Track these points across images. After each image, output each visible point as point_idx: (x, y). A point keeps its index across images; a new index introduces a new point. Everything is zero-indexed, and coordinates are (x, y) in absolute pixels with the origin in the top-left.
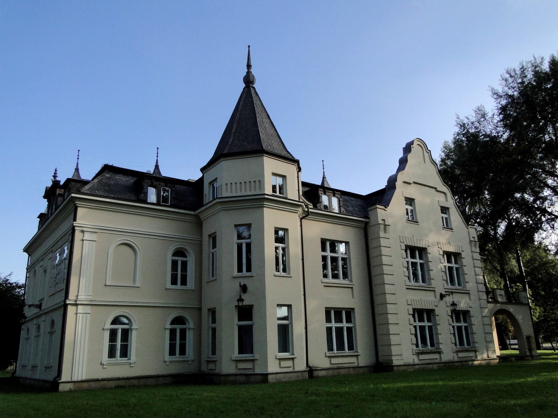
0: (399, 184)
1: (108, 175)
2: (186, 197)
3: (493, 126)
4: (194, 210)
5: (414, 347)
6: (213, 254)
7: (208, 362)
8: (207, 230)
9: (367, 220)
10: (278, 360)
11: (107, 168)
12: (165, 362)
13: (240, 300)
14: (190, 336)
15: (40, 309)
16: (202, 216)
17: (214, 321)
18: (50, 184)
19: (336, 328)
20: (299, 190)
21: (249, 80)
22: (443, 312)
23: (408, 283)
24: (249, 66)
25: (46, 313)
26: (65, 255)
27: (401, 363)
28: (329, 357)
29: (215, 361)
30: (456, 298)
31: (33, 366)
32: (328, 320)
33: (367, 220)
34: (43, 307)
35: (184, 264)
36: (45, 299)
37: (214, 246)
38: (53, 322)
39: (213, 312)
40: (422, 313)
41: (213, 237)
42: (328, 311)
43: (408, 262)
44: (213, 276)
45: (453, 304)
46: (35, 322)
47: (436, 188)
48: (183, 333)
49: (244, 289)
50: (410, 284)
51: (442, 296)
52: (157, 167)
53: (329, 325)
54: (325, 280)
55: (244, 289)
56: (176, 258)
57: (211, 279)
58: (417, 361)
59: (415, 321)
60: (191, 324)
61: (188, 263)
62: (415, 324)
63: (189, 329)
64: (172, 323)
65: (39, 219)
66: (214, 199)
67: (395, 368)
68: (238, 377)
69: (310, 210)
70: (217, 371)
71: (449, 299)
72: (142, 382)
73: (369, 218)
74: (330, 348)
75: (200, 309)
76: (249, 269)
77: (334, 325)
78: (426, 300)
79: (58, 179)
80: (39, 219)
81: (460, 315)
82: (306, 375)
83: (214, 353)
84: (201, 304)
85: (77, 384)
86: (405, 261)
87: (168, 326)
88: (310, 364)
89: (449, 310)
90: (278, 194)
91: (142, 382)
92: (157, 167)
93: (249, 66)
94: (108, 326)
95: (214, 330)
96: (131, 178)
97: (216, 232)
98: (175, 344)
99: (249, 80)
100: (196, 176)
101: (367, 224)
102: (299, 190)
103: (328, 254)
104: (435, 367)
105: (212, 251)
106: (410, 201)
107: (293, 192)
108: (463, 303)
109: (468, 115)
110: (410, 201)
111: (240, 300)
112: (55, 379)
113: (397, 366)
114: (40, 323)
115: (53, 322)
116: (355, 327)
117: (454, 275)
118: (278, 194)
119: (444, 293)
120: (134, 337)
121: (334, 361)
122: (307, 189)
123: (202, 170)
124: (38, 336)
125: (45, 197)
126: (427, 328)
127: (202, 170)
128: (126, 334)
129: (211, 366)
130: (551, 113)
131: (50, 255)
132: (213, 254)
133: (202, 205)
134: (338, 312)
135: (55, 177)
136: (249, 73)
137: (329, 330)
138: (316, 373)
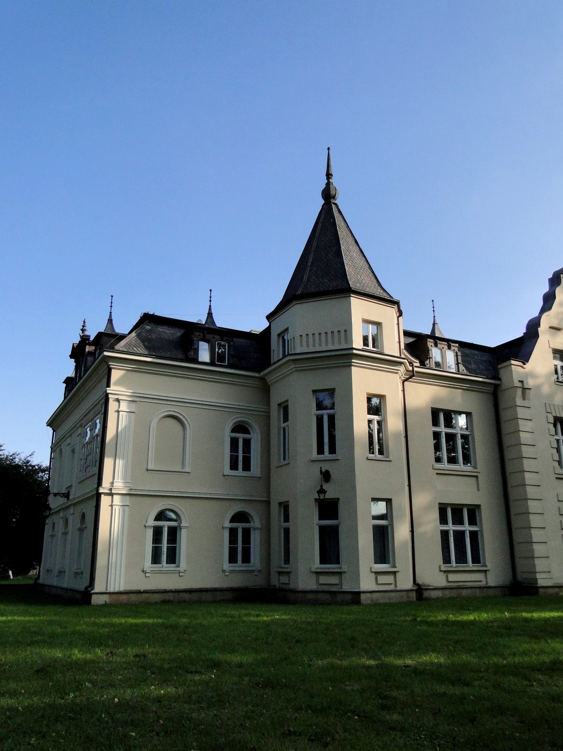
1: (148, 327)
4: (259, 371)
6: (284, 429)
7: (280, 573)
8: (276, 398)
9: (497, 382)
10: (374, 574)
13: (322, 491)
14: (256, 538)
15: (68, 499)
18: (77, 340)
20: (399, 342)
21: (328, 195)
24: (329, 175)
25: (74, 505)
28: (445, 572)
29: (288, 573)
33: (497, 382)
34: (71, 497)
35: (247, 443)
37: (286, 419)
39: (285, 507)
41: (285, 408)
44: (284, 459)
48: (247, 533)
52: (210, 315)
53: (445, 528)
54: (438, 466)
55: (326, 476)
57: (285, 462)
60: (256, 523)
61: (252, 441)
63: (254, 529)
64: (232, 521)
65: (73, 360)
66: (284, 356)
70: (292, 586)
73: (500, 379)
74: (447, 559)
75: (268, 503)
76: (332, 450)
77: (451, 527)
79: (87, 333)
82: (413, 595)
85: (114, 596)
86: (553, 440)
87: (227, 524)
88: (419, 581)
90: (371, 347)
92: (210, 315)
93: (329, 175)
95: (287, 531)
97: (287, 401)
98: (236, 548)
99: (328, 195)
100: (258, 325)
101: (496, 387)
105: (283, 425)
112: (86, 588)
115: (83, 516)
116: (481, 531)
120: (184, 537)
121: (453, 577)
123: (269, 317)
124: (65, 534)
125: (71, 356)
127: (269, 317)
128: (173, 533)
129: (284, 579)
131: (79, 431)
132: (284, 429)
134: (457, 510)
135: (83, 330)
136: (328, 184)
137: (445, 535)
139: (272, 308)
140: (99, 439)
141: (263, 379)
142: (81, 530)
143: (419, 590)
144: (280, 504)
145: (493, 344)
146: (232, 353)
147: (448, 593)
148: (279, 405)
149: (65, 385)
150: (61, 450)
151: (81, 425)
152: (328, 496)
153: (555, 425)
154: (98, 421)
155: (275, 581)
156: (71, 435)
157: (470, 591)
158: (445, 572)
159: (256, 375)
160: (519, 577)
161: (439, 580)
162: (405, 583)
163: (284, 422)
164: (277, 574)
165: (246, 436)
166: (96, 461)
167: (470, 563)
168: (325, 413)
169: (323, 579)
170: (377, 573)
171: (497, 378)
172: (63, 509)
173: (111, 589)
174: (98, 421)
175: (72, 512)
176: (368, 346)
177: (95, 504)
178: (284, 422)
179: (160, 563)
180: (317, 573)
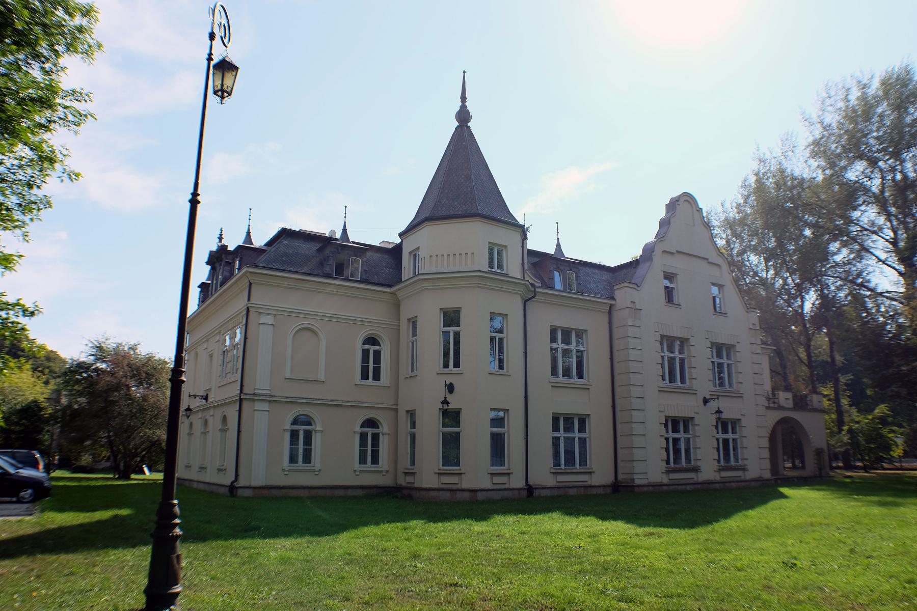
0: (657, 257)
1: (285, 242)
2: (383, 267)
3: (807, 168)
4: (390, 286)
5: (664, 464)
6: (413, 343)
7: (406, 473)
8: (407, 312)
9: (613, 302)
11: (285, 233)
12: (355, 471)
13: (445, 402)
14: (384, 443)
16: (400, 295)
17: (413, 425)
19: (565, 438)
20: (523, 264)
21: (463, 116)
22: (705, 423)
23: (661, 384)
24: (463, 98)
25: (214, 407)
26: (237, 339)
27: (645, 482)
28: (554, 473)
29: (414, 473)
30: (723, 404)
31: (201, 468)
32: (556, 428)
33: (613, 302)
34: (210, 400)
35: (377, 354)
36: (213, 390)
37: (414, 334)
38: (225, 419)
39: (411, 414)
40: (675, 423)
41: (414, 322)
42: (555, 419)
43: (663, 357)
44: (412, 371)
45: (719, 412)
46: (200, 415)
47: (707, 259)
48: (376, 437)
49: (451, 388)
50: (664, 385)
51: (706, 401)
53: (556, 435)
54: (555, 379)
55: (451, 388)
56: (367, 347)
57: (411, 374)
58: (718, 478)
59: (667, 432)
60: (385, 428)
61: (382, 353)
62: (667, 436)
63: (383, 434)
64: (362, 426)
65: (209, 267)
66: (415, 275)
67: (637, 489)
68: (441, 492)
69: (537, 290)
70: (416, 485)
71: (713, 405)
72: (341, 493)
73: (614, 299)
74: (557, 464)
75: (397, 410)
76: (457, 365)
77: (562, 434)
78: (682, 406)
79: (224, 242)
80: (209, 267)
81: (724, 425)
82: (525, 493)
83: (413, 462)
84: (397, 405)
86: (659, 356)
87: (358, 429)
88: (531, 482)
89: (713, 419)
90: (496, 269)
91: (341, 493)
93: (463, 98)
94: (288, 427)
95: (413, 437)
96: (313, 244)
99: (463, 116)
101: (611, 306)
102: (523, 264)
103: (560, 345)
104: (689, 488)
105: (411, 339)
106: (669, 276)
107: (514, 266)
108: (730, 409)
109: (772, 149)
110: (669, 276)
111: (445, 402)
112: (233, 482)
113: (639, 486)
114: (208, 417)
115: (225, 419)
116: (589, 437)
117: (721, 373)
118: (496, 269)
119: (708, 397)
120: (317, 440)
121: (561, 478)
122: (536, 260)
123: (401, 235)
124: (205, 433)
125: (208, 263)
126: (577, 440)
127: (401, 235)
128: (308, 436)
129: (410, 479)
130: (15, 600)
131: (217, 338)
132: (413, 343)
133: (399, 281)
134: (569, 420)
135: (220, 239)
137: (556, 441)
138: (536, 493)
139: (403, 228)
140: (241, 347)
141: (394, 294)
142: (224, 431)
143: (530, 489)
144: (407, 412)
145: (612, 263)
146: (365, 268)
147: (555, 492)
148: (409, 320)
149: (199, 289)
150: (197, 354)
151: (219, 332)
152: (450, 406)
153: (661, 344)
154: (238, 331)
155: (402, 481)
156: (207, 341)
157: (575, 490)
158: (554, 473)
159: (388, 290)
160: (621, 477)
161: (550, 481)
162: (517, 482)
163: (413, 336)
164: (403, 475)
165: (376, 348)
166: (237, 369)
167: (577, 466)
168: (452, 329)
169: (445, 479)
170: (493, 474)
171: (613, 298)
172: (202, 410)
173: (254, 484)
174: (238, 331)
175: (212, 413)
176: (492, 267)
177: (238, 408)
178: (413, 336)
179: (297, 462)
180: (439, 474)
